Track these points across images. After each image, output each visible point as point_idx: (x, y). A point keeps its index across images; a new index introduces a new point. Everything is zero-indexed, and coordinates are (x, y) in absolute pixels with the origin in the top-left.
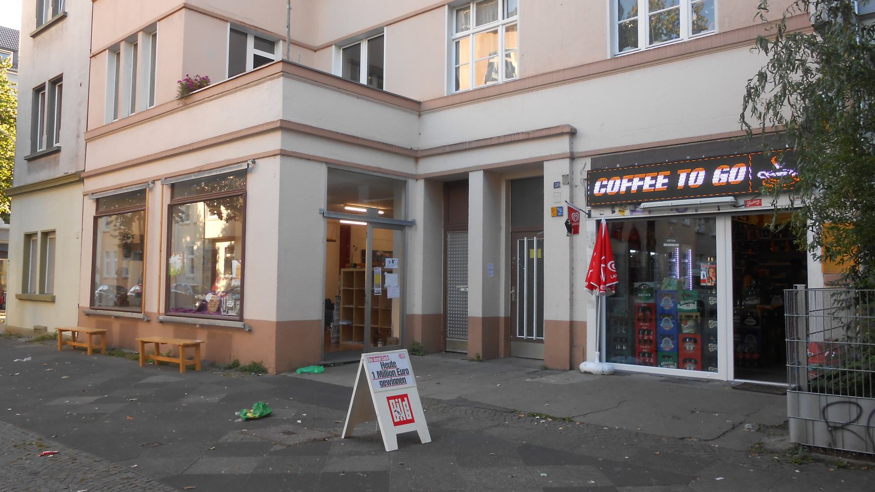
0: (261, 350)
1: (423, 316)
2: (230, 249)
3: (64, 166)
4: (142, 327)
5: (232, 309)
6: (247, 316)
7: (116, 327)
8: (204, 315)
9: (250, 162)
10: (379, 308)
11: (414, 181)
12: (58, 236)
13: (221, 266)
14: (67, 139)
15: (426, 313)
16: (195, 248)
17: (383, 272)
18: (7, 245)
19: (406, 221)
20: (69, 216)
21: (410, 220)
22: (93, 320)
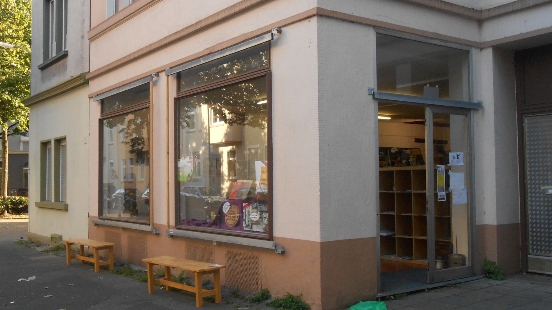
0: (304, 279)
1: (499, 227)
2: (232, 153)
3: (71, 69)
4: (151, 241)
5: (257, 223)
6: (278, 233)
7: (124, 239)
8: (221, 230)
9: (275, 32)
10: (413, 214)
11: (478, 50)
12: (69, 143)
13: (225, 169)
14: (72, 43)
15: (501, 223)
16: (201, 152)
17: (447, 171)
18: (27, 156)
19: (470, 103)
20: (76, 119)
21: (475, 101)
22: (102, 231)
